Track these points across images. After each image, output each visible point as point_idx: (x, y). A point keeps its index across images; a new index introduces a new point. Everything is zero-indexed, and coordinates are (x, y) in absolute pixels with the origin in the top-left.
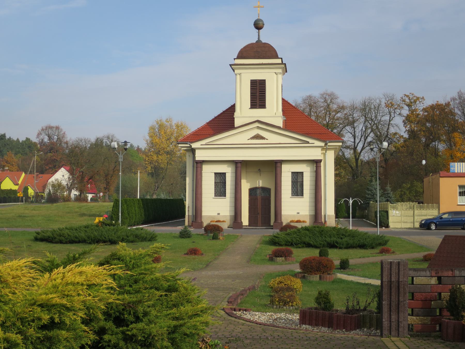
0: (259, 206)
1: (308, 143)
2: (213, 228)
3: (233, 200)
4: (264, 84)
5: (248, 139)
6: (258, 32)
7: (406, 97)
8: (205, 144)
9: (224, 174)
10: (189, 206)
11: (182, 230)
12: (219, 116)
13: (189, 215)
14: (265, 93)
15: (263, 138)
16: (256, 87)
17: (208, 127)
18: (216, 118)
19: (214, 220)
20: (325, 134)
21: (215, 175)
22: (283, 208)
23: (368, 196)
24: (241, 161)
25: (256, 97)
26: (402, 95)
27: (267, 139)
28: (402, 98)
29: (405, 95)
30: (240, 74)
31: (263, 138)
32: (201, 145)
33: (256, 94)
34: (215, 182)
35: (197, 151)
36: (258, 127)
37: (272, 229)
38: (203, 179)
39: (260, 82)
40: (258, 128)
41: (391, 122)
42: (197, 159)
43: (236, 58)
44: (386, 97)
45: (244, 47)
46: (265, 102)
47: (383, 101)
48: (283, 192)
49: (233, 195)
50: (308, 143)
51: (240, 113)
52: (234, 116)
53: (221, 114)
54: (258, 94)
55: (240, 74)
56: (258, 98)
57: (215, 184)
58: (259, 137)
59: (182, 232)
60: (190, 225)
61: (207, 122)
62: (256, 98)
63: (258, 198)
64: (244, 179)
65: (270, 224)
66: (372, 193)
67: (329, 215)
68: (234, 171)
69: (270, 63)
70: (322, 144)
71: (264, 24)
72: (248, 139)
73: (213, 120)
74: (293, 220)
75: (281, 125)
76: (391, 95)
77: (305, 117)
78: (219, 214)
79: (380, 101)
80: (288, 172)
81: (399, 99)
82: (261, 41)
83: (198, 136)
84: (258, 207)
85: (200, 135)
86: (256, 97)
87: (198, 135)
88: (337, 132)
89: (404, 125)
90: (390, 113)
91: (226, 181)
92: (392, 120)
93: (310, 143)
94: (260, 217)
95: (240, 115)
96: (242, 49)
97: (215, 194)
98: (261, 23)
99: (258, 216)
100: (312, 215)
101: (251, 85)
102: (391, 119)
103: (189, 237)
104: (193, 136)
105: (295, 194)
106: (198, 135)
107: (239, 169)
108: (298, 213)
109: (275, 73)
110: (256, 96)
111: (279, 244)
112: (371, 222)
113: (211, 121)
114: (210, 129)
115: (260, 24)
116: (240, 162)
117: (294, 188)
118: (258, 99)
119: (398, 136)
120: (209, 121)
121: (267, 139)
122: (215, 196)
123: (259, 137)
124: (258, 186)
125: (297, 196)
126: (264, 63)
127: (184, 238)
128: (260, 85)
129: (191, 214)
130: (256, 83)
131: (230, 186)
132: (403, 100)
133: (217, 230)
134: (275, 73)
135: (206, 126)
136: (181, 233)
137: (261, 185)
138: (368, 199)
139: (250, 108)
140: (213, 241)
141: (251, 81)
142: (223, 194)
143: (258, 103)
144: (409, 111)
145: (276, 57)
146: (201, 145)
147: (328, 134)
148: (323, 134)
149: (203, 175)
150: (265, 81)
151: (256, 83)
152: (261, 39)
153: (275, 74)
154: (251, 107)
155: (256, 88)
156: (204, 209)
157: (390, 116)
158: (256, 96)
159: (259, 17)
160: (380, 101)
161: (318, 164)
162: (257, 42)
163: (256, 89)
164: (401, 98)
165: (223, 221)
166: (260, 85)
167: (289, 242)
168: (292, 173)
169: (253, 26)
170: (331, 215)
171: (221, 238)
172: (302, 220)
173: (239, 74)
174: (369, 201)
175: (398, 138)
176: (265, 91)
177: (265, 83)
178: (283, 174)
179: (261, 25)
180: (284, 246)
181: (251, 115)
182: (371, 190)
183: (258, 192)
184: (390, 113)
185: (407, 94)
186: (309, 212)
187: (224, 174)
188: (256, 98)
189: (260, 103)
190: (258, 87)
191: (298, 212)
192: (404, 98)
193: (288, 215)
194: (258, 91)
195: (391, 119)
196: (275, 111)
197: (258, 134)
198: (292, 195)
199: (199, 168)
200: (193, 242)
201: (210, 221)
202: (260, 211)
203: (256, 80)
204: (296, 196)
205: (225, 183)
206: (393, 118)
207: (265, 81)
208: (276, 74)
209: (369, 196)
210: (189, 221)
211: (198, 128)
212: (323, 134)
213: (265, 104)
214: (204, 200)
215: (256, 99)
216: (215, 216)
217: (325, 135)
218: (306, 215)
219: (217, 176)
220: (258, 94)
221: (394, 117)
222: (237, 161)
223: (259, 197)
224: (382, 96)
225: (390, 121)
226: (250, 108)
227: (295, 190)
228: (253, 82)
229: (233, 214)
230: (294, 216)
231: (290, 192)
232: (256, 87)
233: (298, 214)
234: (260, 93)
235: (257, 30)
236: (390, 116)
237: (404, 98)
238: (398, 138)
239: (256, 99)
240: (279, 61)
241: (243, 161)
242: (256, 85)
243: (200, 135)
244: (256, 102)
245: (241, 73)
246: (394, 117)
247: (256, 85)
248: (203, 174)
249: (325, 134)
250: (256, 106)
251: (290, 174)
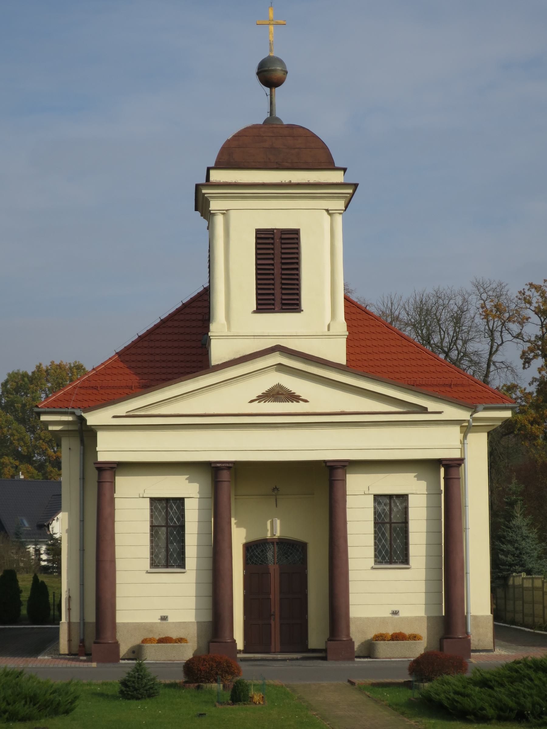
0: (275, 595)
1: (424, 410)
2: (215, 665)
3: (208, 577)
4: (295, 241)
5: (252, 401)
6: (271, 95)
7: (533, 290)
8: (124, 414)
9: (180, 502)
10: (70, 597)
11: (129, 674)
12: (172, 317)
13: (69, 623)
14: (298, 269)
15: (293, 397)
16: (273, 249)
17: (121, 365)
18: (141, 338)
19: (151, 636)
20: (462, 385)
21: (151, 505)
22: (353, 599)
23: (506, 556)
24: (230, 465)
25: (273, 279)
26: (522, 286)
27: (306, 401)
28: (524, 294)
29: (531, 285)
30: (225, 213)
31: (293, 397)
32: (114, 417)
33: (272, 272)
34: (152, 527)
35: (101, 436)
36: (280, 364)
37: (325, 659)
38: (117, 518)
39: (284, 236)
40: (280, 368)
41: (494, 358)
42: (102, 457)
43: (213, 165)
44: (482, 290)
45: (234, 136)
46: (299, 294)
47: (475, 303)
48: (352, 552)
49: (208, 564)
50: (424, 410)
51: (225, 323)
52: (210, 334)
53: (157, 327)
54: (277, 271)
55: (225, 213)
56: (278, 282)
57: (152, 530)
58: (282, 394)
59: (129, 681)
60: (75, 650)
61: (118, 351)
62: (272, 282)
63: (272, 571)
64: (233, 517)
65: (307, 645)
66: (517, 549)
67: (475, 617)
68: (208, 491)
69: (312, 181)
70: (463, 415)
71: (287, 72)
72: (252, 401)
73: (135, 344)
74: (383, 631)
75: (343, 360)
76: (494, 286)
77: (398, 337)
78: (164, 618)
79: (465, 300)
80: (365, 494)
81: (515, 296)
82: (278, 119)
83: (95, 391)
84: (272, 597)
85: (102, 387)
86: (273, 279)
87: (450, 386)
88: (11, 388)
89: (524, 364)
90: (492, 332)
91: (184, 521)
92: (497, 350)
93: (429, 410)
94: (275, 624)
95: (226, 332)
96: (228, 141)
97: (152, 559)
98: (279, 68)
99: (272, 622)
100: (436, 617)
101: (257, 243)
102: (494, 349)
103: (150, 696)
104: (82, 391)
105: (384, 558)
106: (95, 388)
107: (225, 487)
108: (395, 613)
109: (327, 210)
110: (272, 277)
111: (475, 715)
112: (536, 631)
113: (127, 348)
114: (128, 371)
115: (275, 70)
116: (229, 468)
117: (380, 540)
118: (278, 286)
119: (519, 394)
120: (122, 348)
121: (306, 401)
122: (154, 564)
123: (282, 394)
124: (269, 535)
125: (391, 563)
126: (294, 181)
127: (138, 699)
128: (283, 246)
129: (75, 619)
130: (273, 238)
131: (196, 536)
132: (525, 299)
133: (227, 672)
134: (327, 210)
135: (115, 361)
136: (124, 683)
137: (278, 534)
138: (505, 565)
139: (254, 312)
140: (236, 707)
141: (256, 234)
142: (175, 561)
143: (278, 296)
144: (542, 327)
145: (329, 165)
146: (114, 417)
147: (469, 385)
148: (456, 385)
149: (118, 503)
150: (296, 232)
151: (273, 238)
152: (278, 114)
153: (325, 213)
154: (257, 309)
155: (273, 254)
156: (121, 604)
157: (493, 340)
158: (272, 277)
159: (271, 50)
160: (465, 300)
161: (453, 471)
162: (266, 122)
163: (272, 256)
164: (520, 292)
165: (180, 640)
166: (283, 246)
167: (511, 710)
168: (377, 498)
169: (256, 79)
170: (482, 616)
171: (256, 698)
172: (407, 631)
173: (223, 214)
174: (508, 570)
175: (521, 398)
176: (298, 263)
177: (298, 239)
178: (350, 501)
179: (279, 74)
180: (494, 721)
181: (258, 332)
182: (511, 542)
183: (271, 554)
184: (492, 332)
185: (536, 283)
186: (426, 610)
187: (180, 502)
188: (272, 282)
189: (284, 297)
190: (277, 251)
191: (395, 608)
192: (527, 293)
193: (368, 619)
194: (277, 261)
195: (494, 349)
196: (328, 319)
197: (279, 386)
198: (376, 562)
199: (108, 484)
200: (201, 715)
201: (142, 638)
202: (275, 608)
203: (272, 230)
204: (387, 563)
205: (182, 527)
206: (499, 346)
207: (296, 232)
208: (330, 214)
209: (509, 559)
210: (69, 641)
211: (94, 369)
212: (456, 385)
213: (299, 300)
214: (121, 577)
215: (273, 284)
216: (152, 625)
217: (461, 389)
218: (421, 617)
219: (156, 508)
220: (277, 271)
221: (501, 345)
222: (219, 465)
223: (273, 567)
224: (470, 288)
225: (491, 354)
226: (254, 312)
227: (384, 546)
228: (263, 236)
229: (207, 617)
230: (383, 620)
231: (371, 552)
232: (273, 249)
233: (396, 616)
234: (284, 267)
235: (268, 90)
236: (493, 340)
237: (527, 293)
238: (521, 398)
239: (273, 284)
240: (336, 177)
241: (235, 463)
242: (273, 244)
243: (102, 387)
244: (273, 294)
245: (227, 210)
246: (503, 343)
247: (273, 244)
248: (117, 501)
249: (462, 385)
250: (273, 304)
251: (370, 502)
